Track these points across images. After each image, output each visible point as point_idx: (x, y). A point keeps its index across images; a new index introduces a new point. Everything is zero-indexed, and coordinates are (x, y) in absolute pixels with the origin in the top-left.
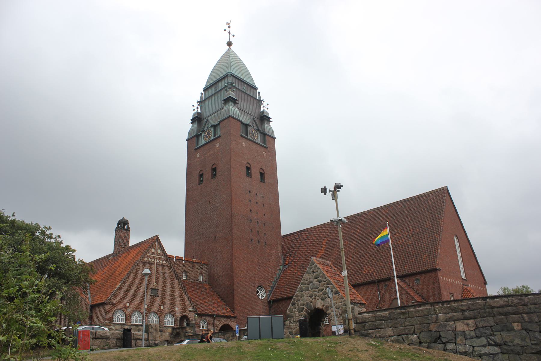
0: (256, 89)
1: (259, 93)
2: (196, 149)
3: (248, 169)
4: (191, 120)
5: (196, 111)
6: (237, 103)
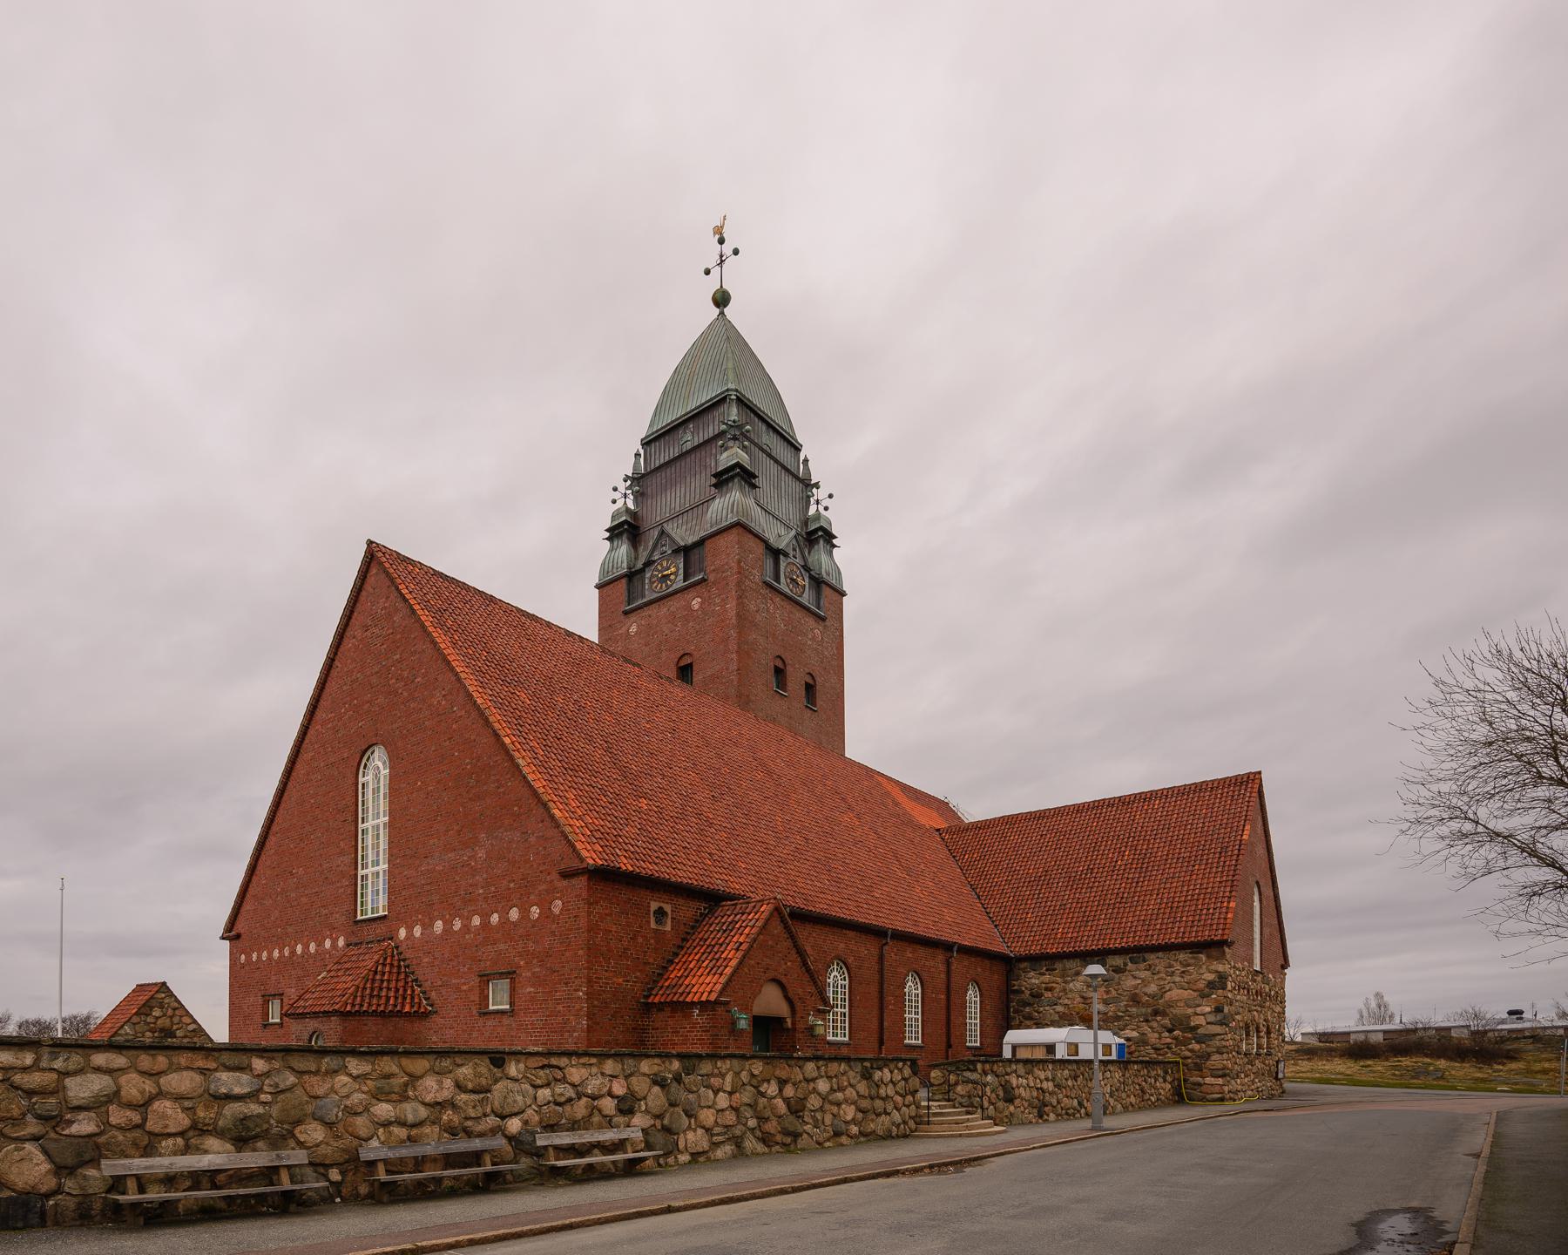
0: (797, 449)
1: (806, 461)
2: (626, 613)
3: (779, 672)
5: (620, 503)
6: (754, 486)
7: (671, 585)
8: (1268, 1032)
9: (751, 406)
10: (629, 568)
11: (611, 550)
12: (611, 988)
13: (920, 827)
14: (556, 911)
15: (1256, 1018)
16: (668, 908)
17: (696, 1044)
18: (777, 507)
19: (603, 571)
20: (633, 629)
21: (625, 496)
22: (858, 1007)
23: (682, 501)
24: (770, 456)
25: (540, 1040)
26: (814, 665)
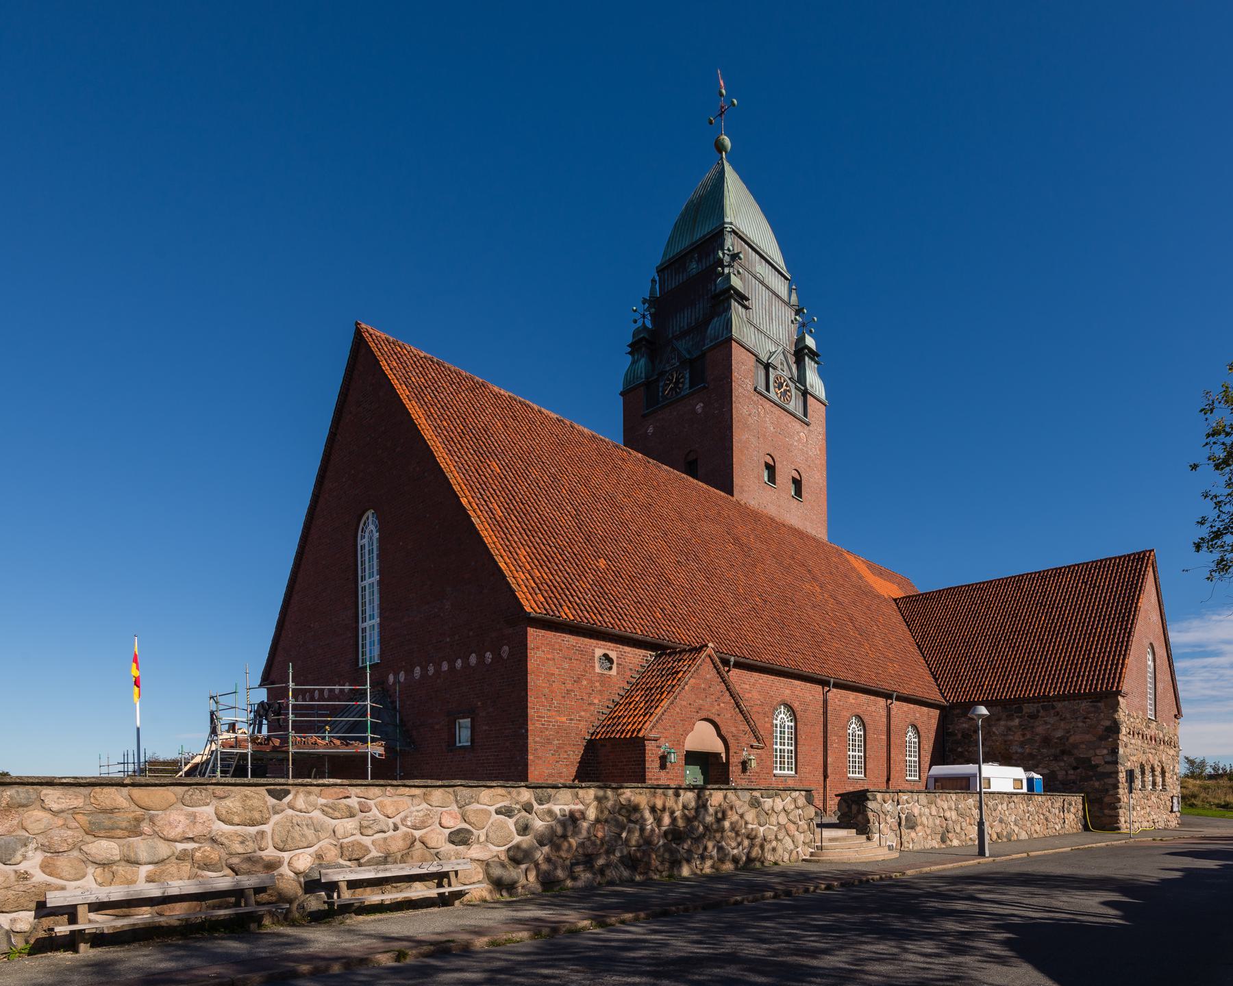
2: (644, 416)
3: (771, 469)
4: (628, 346)
5: (640, 324)
7: (680, 392)
8: (1163, 773)
9: (746, 238)
10: (647, 378)
11: (634, 363)
12: (554, 726)
13: (879, 596)
14: (505, 656)
15: (1151, 759)
16: (613, 655)
17: (631, 776)
18: (768, 327)
19: (627, 381)
20: (651, 430)
21: (644, 316)
22: (804, 745)
23: (689, 321)
24: (762, 283)
25: (492, 774)
26: (800, 463)
